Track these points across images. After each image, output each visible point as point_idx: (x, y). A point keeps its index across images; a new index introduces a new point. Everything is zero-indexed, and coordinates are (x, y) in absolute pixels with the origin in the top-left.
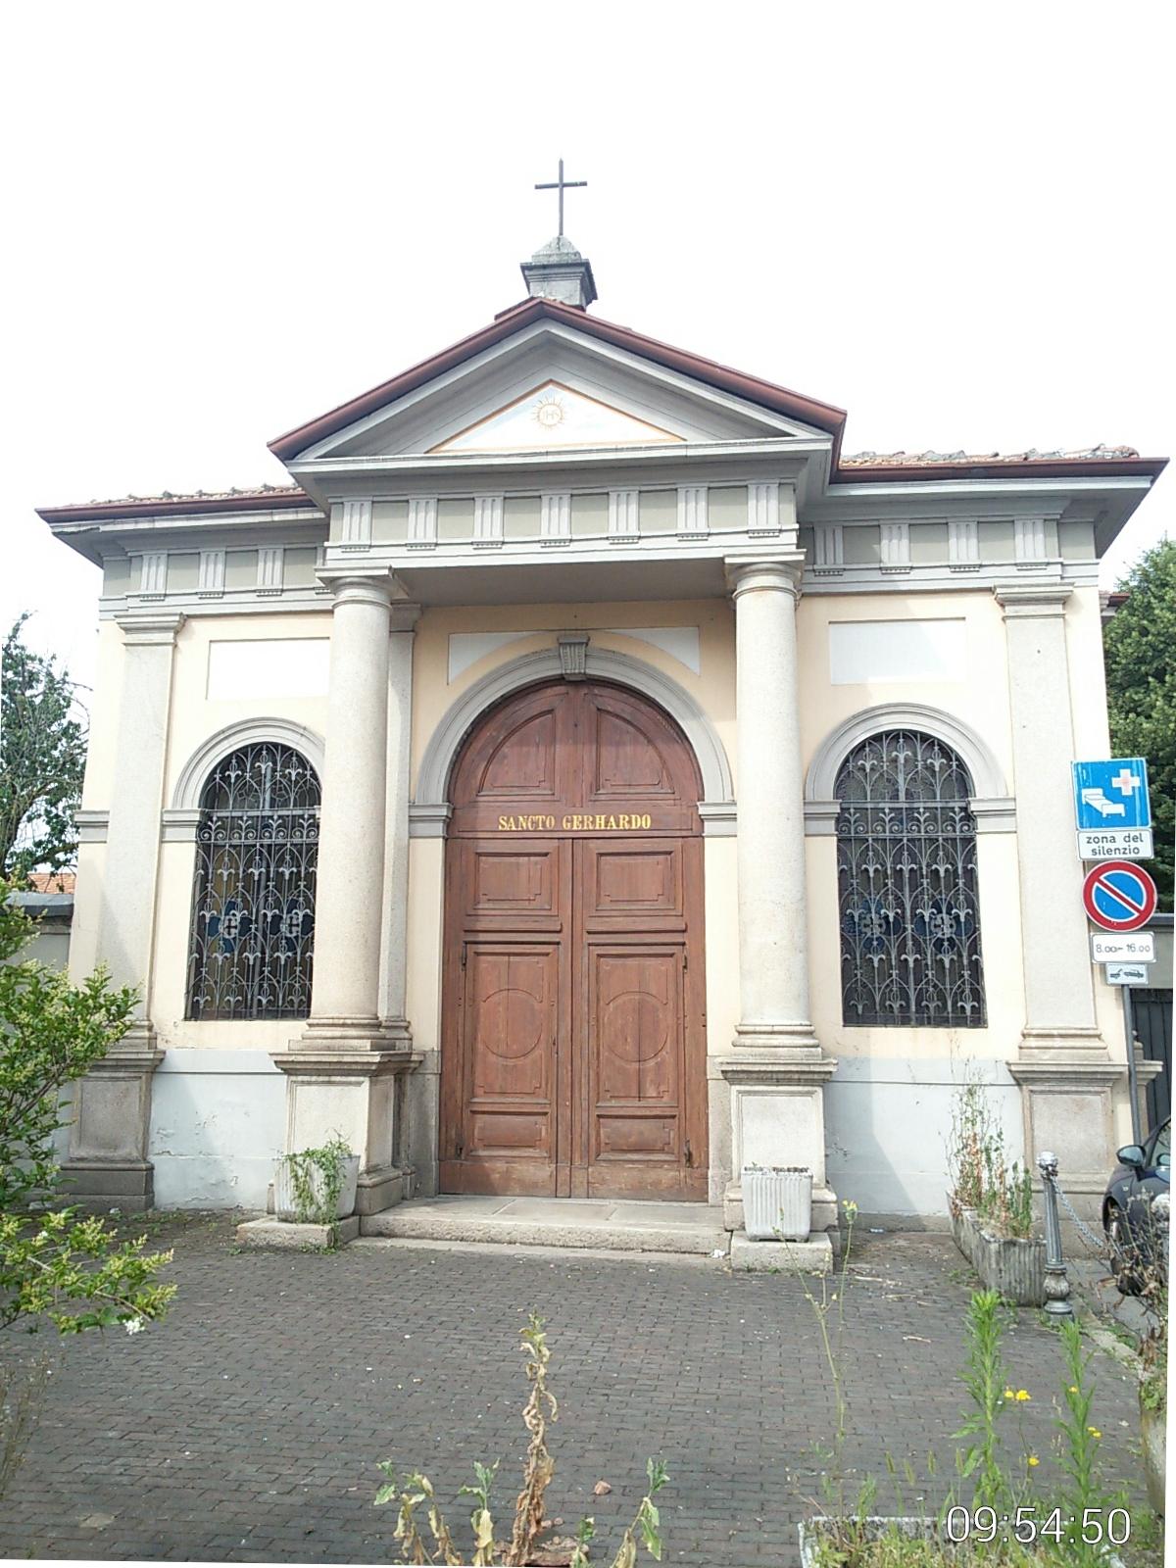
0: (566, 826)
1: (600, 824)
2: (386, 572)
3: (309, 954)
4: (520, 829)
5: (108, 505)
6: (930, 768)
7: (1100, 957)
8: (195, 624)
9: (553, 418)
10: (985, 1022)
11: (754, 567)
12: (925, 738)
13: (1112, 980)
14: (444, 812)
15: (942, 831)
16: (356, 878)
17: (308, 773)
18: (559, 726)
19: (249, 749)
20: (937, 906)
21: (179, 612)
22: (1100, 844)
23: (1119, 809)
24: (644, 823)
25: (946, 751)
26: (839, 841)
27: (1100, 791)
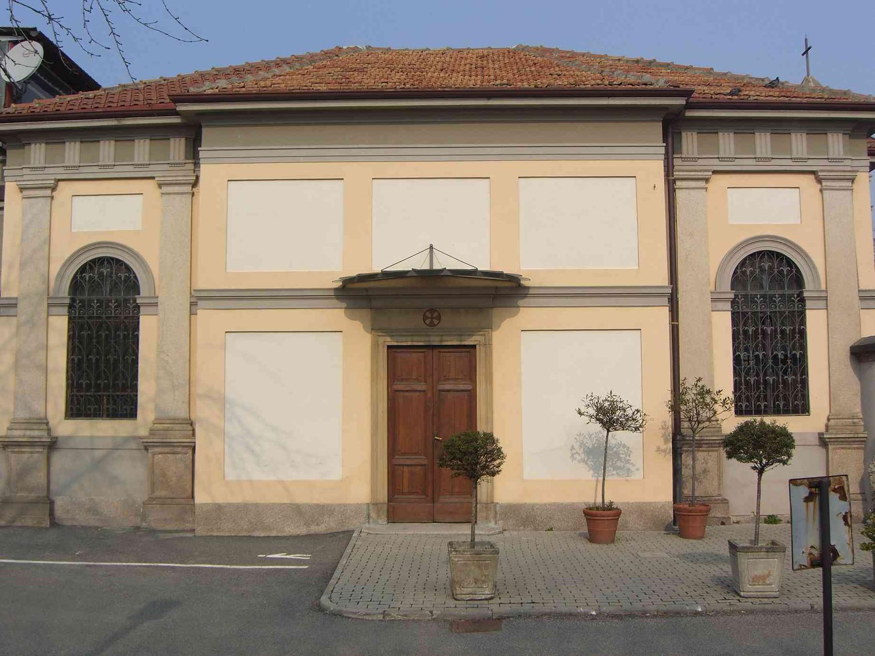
3: (135, 382)
6: (781, 272)
8: (61, 184)
10: (808, 411)
17: (132, 276)
19: (97, 260)
21: (53, 178)
25: (790, 263)
26: (733, 314)
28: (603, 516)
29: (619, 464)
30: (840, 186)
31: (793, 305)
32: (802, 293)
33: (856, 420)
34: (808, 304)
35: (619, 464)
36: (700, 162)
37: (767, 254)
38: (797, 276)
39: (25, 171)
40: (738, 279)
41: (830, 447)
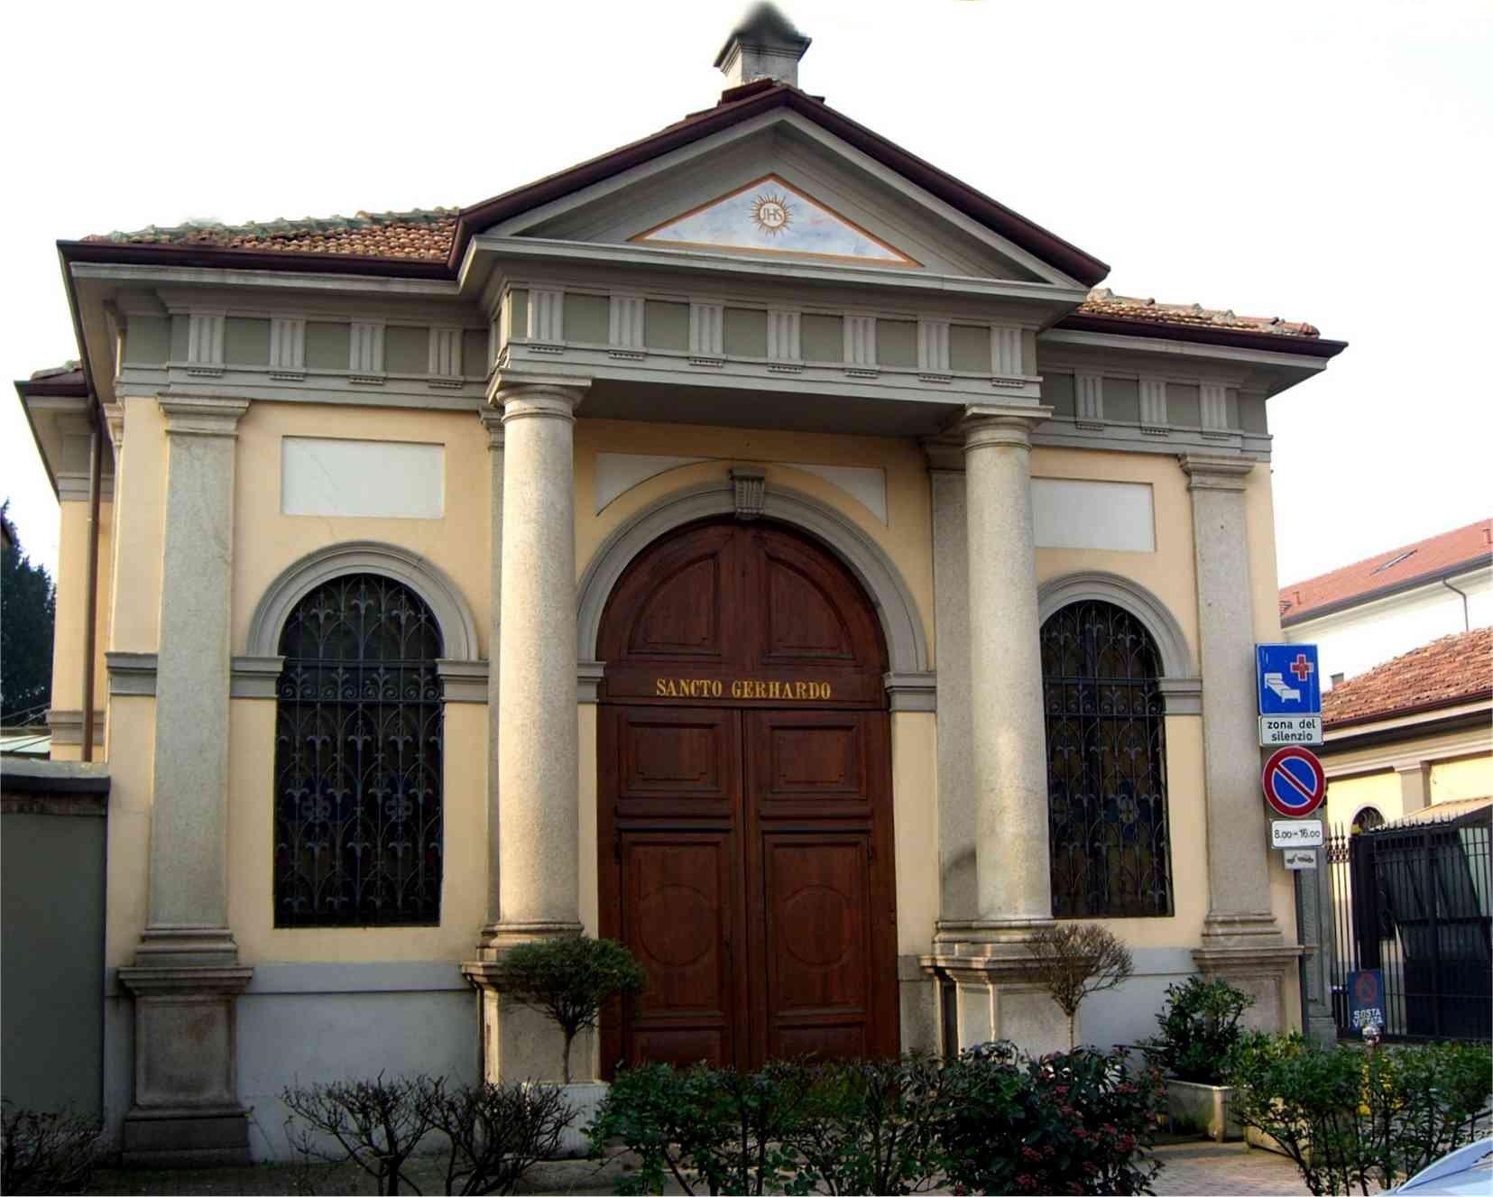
0: (735, 693)
1: (774, 693)
2: (588, 383)
4: (681, 695)
5: (153, 246)
7: (1277, 842)
9: (775, 219)
11: (999, 420)
12: (391, 584)
13: (1288, 866)
14: (599, 673)
15: (363, 697)
16: (564, 756)
18: (724, 573)
20: (310, 784)
22: (1279, 729)
23: (1295, 694)
24: (823, 692)
25: (415, 601)
27: (1280, 675)
32: (1156, 684)
34: (1170, 705)
38: (1148, 652)
39: (173, 376)
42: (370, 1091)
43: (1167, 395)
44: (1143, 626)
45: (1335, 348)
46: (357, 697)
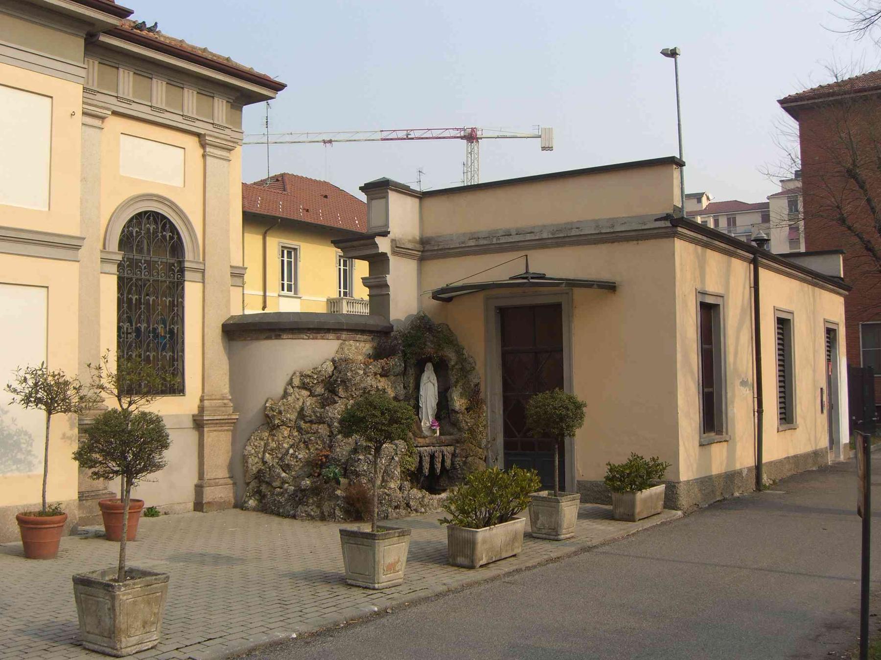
25: (173, 229)
28: (54, 523)
29: (19, 456)
30: (221, 155)
31: (140, 271)
33: (226, 401)
34: (188, 275)
35: (19, 456)
36: (99, 97)
37: (153, 215)
40: (126, 242)
41: (206, 429)
42: (307, 482)
43: (197, 98)
44: (176, 229)
45: (278, 87)
46: (150, 276)
